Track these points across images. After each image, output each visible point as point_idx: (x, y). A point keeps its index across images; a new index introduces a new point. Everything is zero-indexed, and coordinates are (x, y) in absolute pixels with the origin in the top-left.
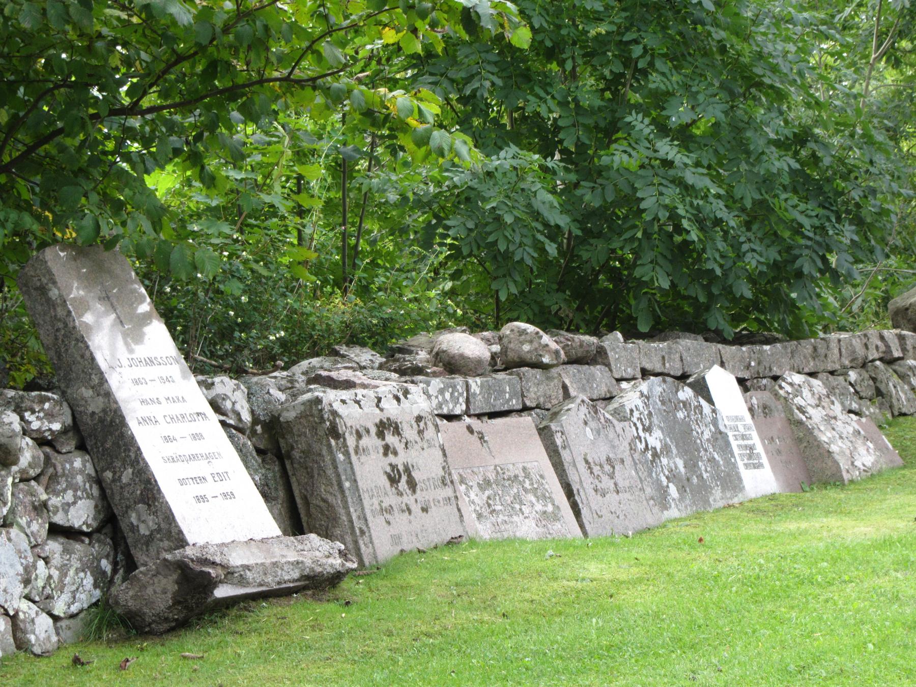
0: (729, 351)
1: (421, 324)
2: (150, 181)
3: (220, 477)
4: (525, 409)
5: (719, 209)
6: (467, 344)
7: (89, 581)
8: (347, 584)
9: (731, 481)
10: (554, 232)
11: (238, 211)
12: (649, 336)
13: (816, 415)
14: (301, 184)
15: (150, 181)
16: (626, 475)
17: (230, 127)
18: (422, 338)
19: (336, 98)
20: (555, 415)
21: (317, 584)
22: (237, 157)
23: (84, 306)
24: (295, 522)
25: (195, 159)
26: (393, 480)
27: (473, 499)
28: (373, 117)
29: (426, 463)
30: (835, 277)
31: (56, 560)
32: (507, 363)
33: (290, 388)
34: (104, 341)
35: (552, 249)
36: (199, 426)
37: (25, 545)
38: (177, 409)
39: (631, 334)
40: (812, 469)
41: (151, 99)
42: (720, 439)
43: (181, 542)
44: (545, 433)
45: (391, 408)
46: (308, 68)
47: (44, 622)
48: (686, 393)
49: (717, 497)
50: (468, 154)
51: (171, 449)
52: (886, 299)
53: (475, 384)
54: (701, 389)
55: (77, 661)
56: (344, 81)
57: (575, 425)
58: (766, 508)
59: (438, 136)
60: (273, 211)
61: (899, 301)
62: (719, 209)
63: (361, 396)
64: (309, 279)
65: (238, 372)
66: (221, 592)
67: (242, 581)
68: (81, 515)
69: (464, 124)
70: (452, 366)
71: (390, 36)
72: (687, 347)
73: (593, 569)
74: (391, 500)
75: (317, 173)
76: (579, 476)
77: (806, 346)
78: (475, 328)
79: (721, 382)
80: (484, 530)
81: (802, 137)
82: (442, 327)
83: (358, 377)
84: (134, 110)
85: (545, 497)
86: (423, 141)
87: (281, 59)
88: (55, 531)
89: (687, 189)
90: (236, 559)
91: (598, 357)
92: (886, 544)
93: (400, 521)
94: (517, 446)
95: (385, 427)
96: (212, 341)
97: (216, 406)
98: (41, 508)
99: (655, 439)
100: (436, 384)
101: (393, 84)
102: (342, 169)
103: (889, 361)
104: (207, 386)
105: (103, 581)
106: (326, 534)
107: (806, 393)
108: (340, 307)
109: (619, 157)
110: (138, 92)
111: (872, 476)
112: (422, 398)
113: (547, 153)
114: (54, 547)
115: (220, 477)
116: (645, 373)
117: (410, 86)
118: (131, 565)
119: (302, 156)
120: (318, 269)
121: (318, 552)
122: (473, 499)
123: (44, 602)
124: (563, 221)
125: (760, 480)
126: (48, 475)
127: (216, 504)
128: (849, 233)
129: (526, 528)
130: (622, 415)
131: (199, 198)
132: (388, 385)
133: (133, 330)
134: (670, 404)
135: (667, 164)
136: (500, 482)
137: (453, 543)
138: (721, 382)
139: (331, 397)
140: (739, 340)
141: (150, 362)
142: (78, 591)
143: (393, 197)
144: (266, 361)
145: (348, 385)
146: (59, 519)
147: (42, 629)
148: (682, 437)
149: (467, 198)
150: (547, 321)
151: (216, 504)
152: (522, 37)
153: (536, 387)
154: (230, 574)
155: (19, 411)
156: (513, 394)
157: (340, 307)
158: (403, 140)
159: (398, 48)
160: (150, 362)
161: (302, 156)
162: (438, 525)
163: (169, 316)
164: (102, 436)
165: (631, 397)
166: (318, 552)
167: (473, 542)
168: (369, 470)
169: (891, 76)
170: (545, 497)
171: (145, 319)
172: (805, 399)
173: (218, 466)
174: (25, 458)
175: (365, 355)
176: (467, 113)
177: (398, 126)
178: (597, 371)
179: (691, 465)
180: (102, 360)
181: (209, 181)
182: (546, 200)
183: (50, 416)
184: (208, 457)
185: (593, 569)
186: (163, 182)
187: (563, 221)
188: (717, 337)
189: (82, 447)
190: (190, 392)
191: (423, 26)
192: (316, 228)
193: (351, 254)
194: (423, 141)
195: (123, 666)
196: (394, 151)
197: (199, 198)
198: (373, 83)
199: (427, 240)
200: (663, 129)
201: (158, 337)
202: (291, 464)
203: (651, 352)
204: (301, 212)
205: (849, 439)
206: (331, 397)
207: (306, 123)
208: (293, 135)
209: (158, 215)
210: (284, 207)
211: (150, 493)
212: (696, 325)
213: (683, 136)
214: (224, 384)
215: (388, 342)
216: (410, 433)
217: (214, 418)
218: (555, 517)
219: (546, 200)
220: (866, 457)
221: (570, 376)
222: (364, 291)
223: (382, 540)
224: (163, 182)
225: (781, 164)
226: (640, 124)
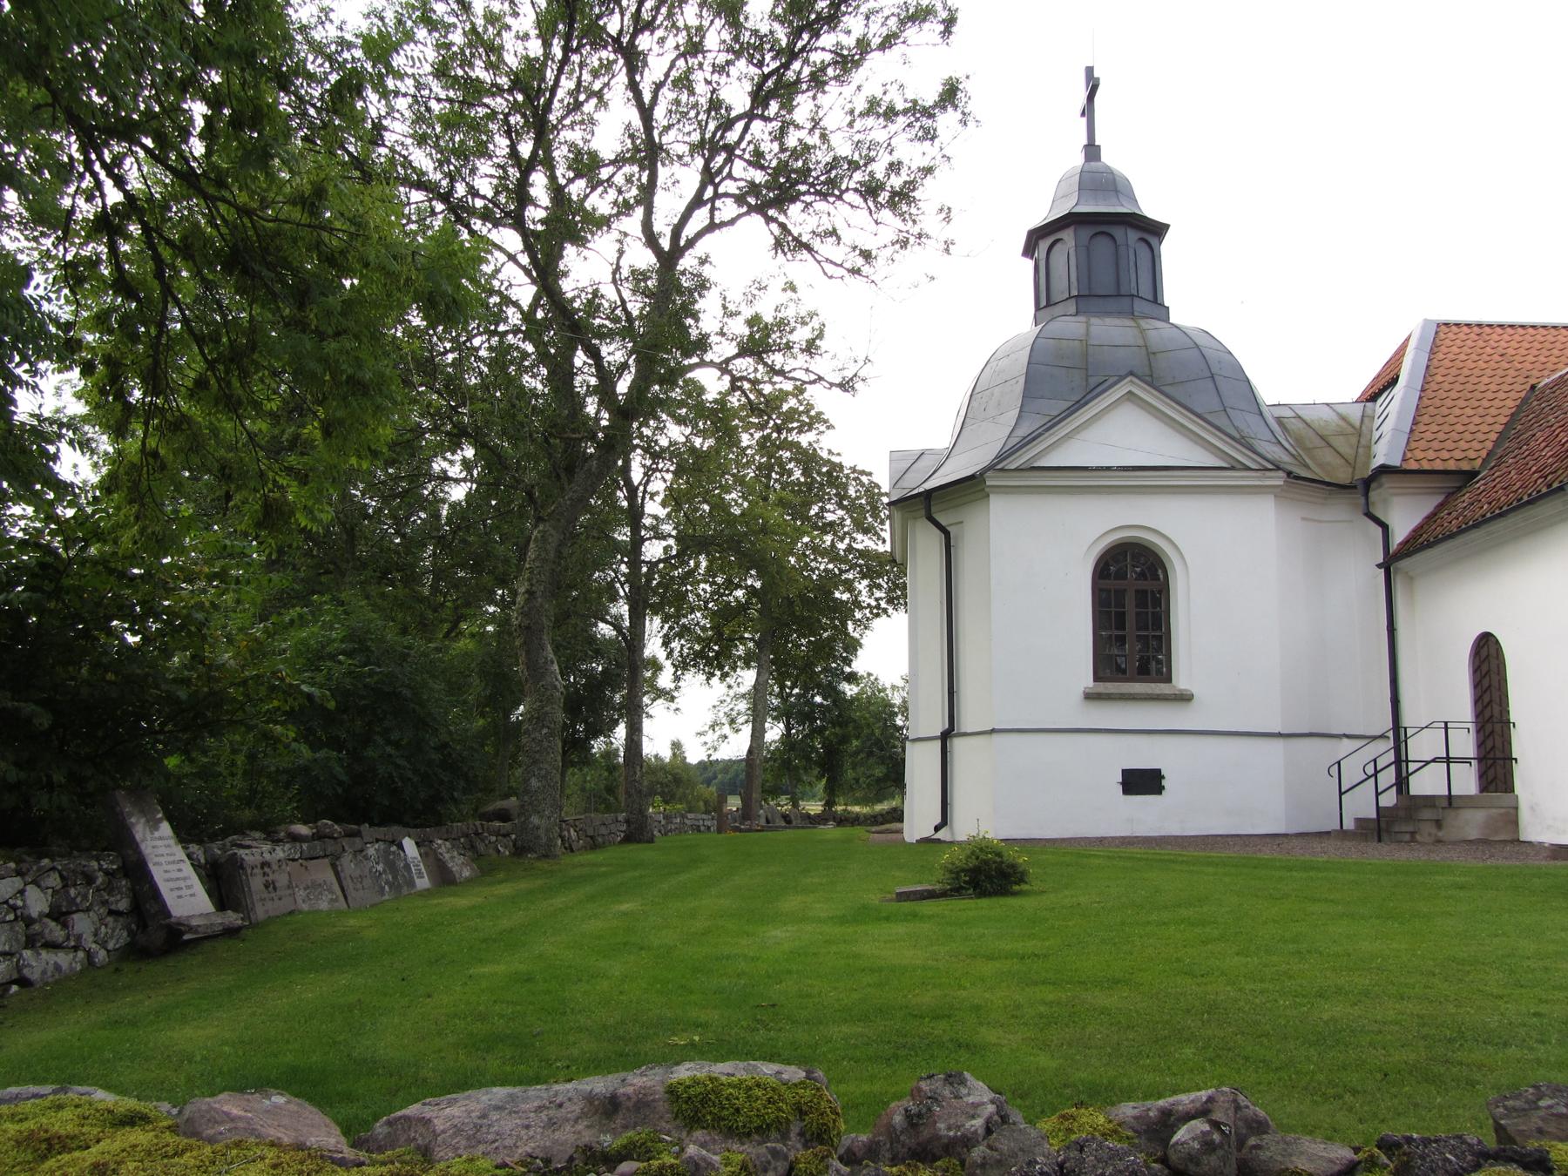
0: (412, 831)
1: (283, 821)
2: (166, 761)
3: (189, 887)
4: (326, 856)
5: (410, 774)
6: (303, 829)
7: (125, 934)
8: (243, 932)
9: (411, 884)
10: (340, 783)
11: (205, 774)
12: (379, 825)
13: (447, 856)
14: (233, 764)
15: (166, 761)
16: (368, 882)
17: (203, 739)
18: (283, 827)
19: (250, 728)
20: (338, 858)
21: (231, 932)
22: (205, 752)
23: (130, 815)
24: (221, 903)
25: (186, 752)
26: (267, 887)
27: (301, 894)
28: (266, 736)
29: (282, 879)
30: (455, 801)
31: (111, 925)
32: (318, 836)
33: (223, 848)
34: (140, 830)
35: (340, 791)
36: (181, 866)
37: (96, 918)
38: (171, 859)
39: (372, 825)
40: (444, 878)
41: (169, 727)
42: (407, 867)
43: (169, 915)
44: (334, 866)
45: (267, 856)
46: (240, 715)
47: (102, 954)
48: (394, 848)
49: (405, 891)
50: (305, 751)
51: (167, 876)
52: (476, 810)
53: (305, 846)
54: (401, 847)
55: (117, 970)
56: (255, 722)
57: (348, 864)
58: (426, 894)
59: (294, 745)
60: (220, 774)
61: (482, 810)
62: (410, 774)
63: (256, 852)
64: (235, 803)
65: (200, 842)
66: (186, 937)
67: (196, 932)
68: (123, 905)
69: (307, 741)
70: (295, 838)
71: (276, 703)
72: (395, 829)
73: (352, 922)
74: (265, 895)
75: (240, 759)
76: (348, 883)
77: (444, 829)
78: (305, 823)
79: (409, 844)
80: (305, 907)
81: (445, 746)
82: (292, 822)
83: (254, 844)
84: (161, 732)
85: (332, 892)
86: (287, 746)
87: (227, 712)
88: (111, 913)
89: (398, 766)
90: (194, 923)
91: (358, 834)
92: (473, 907)
93: (269, 905)
94: (322, 872)
95: (265, 864)
96: (186, 833)
97: (189, 856)
98: (105, 903)
99: (380, 868)
100: (287, 846)
101: (276, 723)
102: (252, 757)
103: (477, 834)
104: (185, 848)
105: (131, 933)
106: (235, 910)
107: (443, 847)
108: (248, 814)
109: (370, 753)
110: (163, 724)
111: (469, 881)
112: (280, 853)
113: (340, 751)
114: (110, 919)
115: (189, 887)
116: (377, 841)
117: (282, 724)
118: (145, 926)
119: (234, 751)
120: (706, 803)
121: (232, 918)
122: (301, 894)
123: (103, 944)
124: (344, 778)
125: (423, 883)
126: (109, 888)
127: (182, 890)
128: (462, 783)
129: (324, 905)
130: (367, 858)
131: (187, 769)
132: (266, 847)
133: (155, 826)
134: (387, 852)
135: (390, 756)
136: (314, 887)
137: (291, 913)
138: (409, 844)
139: (242, 852)
140: (416, 827)
141: (161, 838)
142: (119, 938)
143: (273, 769)
144: (213, 837)
145: (249, 847)
146: (113, 907)
147: (101, 955)
148: (391, 866)
149: (305, 770)
150: (337, 820)
151: (182, 890)
152: (332, 705)
153: (331, 847)
154: (191, 929)
155: (98, 860)
156: (322, 849)
157: (248, 814)
158: (280, 746)
159: (279, 708)
160: (161, 838)
161: (234, 751)
162: (285, 905)
163: (170, 818)
164: (137, 871)
165: (371, 851)
166: (232, 918)
167: (301, 912)
168: (256, 883)
169: (481, 722)
170: (332, 892)
171: (160, 821)
172: (443, 850)
173: (189, 883)
174: (99, 881)
175: (257, 835)
176: (307, 736)
177: (277, 740)
178: (357, 840)
179: (395, 877)
180: (138, 837)
181: (192, 761)
182: (338, 769)
183: (112, 862)
184: (185, 879)
185: (352, 922)
186: (172, 762)
187: (344, 778)
188: (406, 825)
189: (126, 876)
190: (180, 853)
191: (290, 700)
192: (239, 783)
193: (254, 792)
194: (287, 746)
195: (139, 970)
196: (275, 749)
197: (187, 769)
198: (267, 722)
199: (287, 786)
200: (389, 742)
201: (166, 828)
202: (222, 881)
203: (381, 831)
204: (233, 775)
205: (460, 866)
206: (242, 852)
207: (238, 738)
208: (231, 743)
209: (168, 775)
210: (225, 773)
211: (156, 894)
212: (399, 821)
213: (397, 745)
214: (194, 848)
215: (270, 832)
216: (275, 867)
217: (188, 862)
218: (336, 900)
219: (338, 769)
220: (466, 873)
221: (345, 842)
222: (259, 808)
223: (260, 912)
224: (172, 762)
225: (436, 756)
226: (379, 740)
